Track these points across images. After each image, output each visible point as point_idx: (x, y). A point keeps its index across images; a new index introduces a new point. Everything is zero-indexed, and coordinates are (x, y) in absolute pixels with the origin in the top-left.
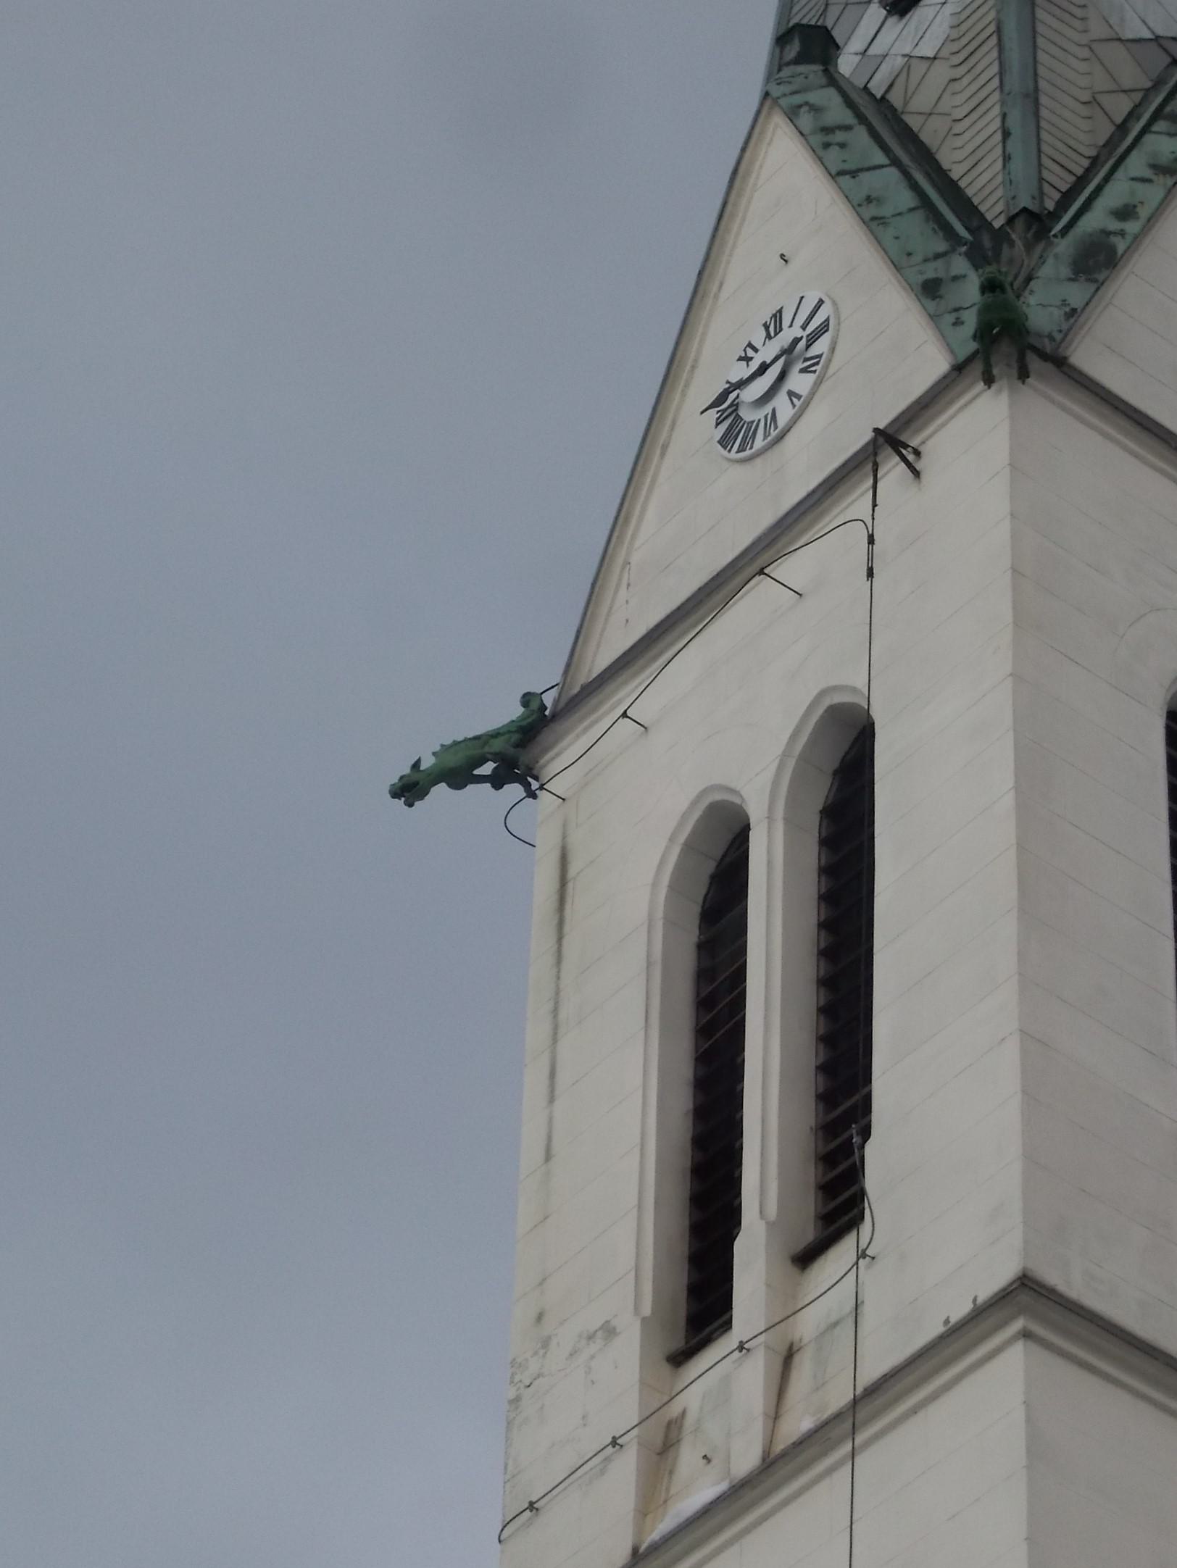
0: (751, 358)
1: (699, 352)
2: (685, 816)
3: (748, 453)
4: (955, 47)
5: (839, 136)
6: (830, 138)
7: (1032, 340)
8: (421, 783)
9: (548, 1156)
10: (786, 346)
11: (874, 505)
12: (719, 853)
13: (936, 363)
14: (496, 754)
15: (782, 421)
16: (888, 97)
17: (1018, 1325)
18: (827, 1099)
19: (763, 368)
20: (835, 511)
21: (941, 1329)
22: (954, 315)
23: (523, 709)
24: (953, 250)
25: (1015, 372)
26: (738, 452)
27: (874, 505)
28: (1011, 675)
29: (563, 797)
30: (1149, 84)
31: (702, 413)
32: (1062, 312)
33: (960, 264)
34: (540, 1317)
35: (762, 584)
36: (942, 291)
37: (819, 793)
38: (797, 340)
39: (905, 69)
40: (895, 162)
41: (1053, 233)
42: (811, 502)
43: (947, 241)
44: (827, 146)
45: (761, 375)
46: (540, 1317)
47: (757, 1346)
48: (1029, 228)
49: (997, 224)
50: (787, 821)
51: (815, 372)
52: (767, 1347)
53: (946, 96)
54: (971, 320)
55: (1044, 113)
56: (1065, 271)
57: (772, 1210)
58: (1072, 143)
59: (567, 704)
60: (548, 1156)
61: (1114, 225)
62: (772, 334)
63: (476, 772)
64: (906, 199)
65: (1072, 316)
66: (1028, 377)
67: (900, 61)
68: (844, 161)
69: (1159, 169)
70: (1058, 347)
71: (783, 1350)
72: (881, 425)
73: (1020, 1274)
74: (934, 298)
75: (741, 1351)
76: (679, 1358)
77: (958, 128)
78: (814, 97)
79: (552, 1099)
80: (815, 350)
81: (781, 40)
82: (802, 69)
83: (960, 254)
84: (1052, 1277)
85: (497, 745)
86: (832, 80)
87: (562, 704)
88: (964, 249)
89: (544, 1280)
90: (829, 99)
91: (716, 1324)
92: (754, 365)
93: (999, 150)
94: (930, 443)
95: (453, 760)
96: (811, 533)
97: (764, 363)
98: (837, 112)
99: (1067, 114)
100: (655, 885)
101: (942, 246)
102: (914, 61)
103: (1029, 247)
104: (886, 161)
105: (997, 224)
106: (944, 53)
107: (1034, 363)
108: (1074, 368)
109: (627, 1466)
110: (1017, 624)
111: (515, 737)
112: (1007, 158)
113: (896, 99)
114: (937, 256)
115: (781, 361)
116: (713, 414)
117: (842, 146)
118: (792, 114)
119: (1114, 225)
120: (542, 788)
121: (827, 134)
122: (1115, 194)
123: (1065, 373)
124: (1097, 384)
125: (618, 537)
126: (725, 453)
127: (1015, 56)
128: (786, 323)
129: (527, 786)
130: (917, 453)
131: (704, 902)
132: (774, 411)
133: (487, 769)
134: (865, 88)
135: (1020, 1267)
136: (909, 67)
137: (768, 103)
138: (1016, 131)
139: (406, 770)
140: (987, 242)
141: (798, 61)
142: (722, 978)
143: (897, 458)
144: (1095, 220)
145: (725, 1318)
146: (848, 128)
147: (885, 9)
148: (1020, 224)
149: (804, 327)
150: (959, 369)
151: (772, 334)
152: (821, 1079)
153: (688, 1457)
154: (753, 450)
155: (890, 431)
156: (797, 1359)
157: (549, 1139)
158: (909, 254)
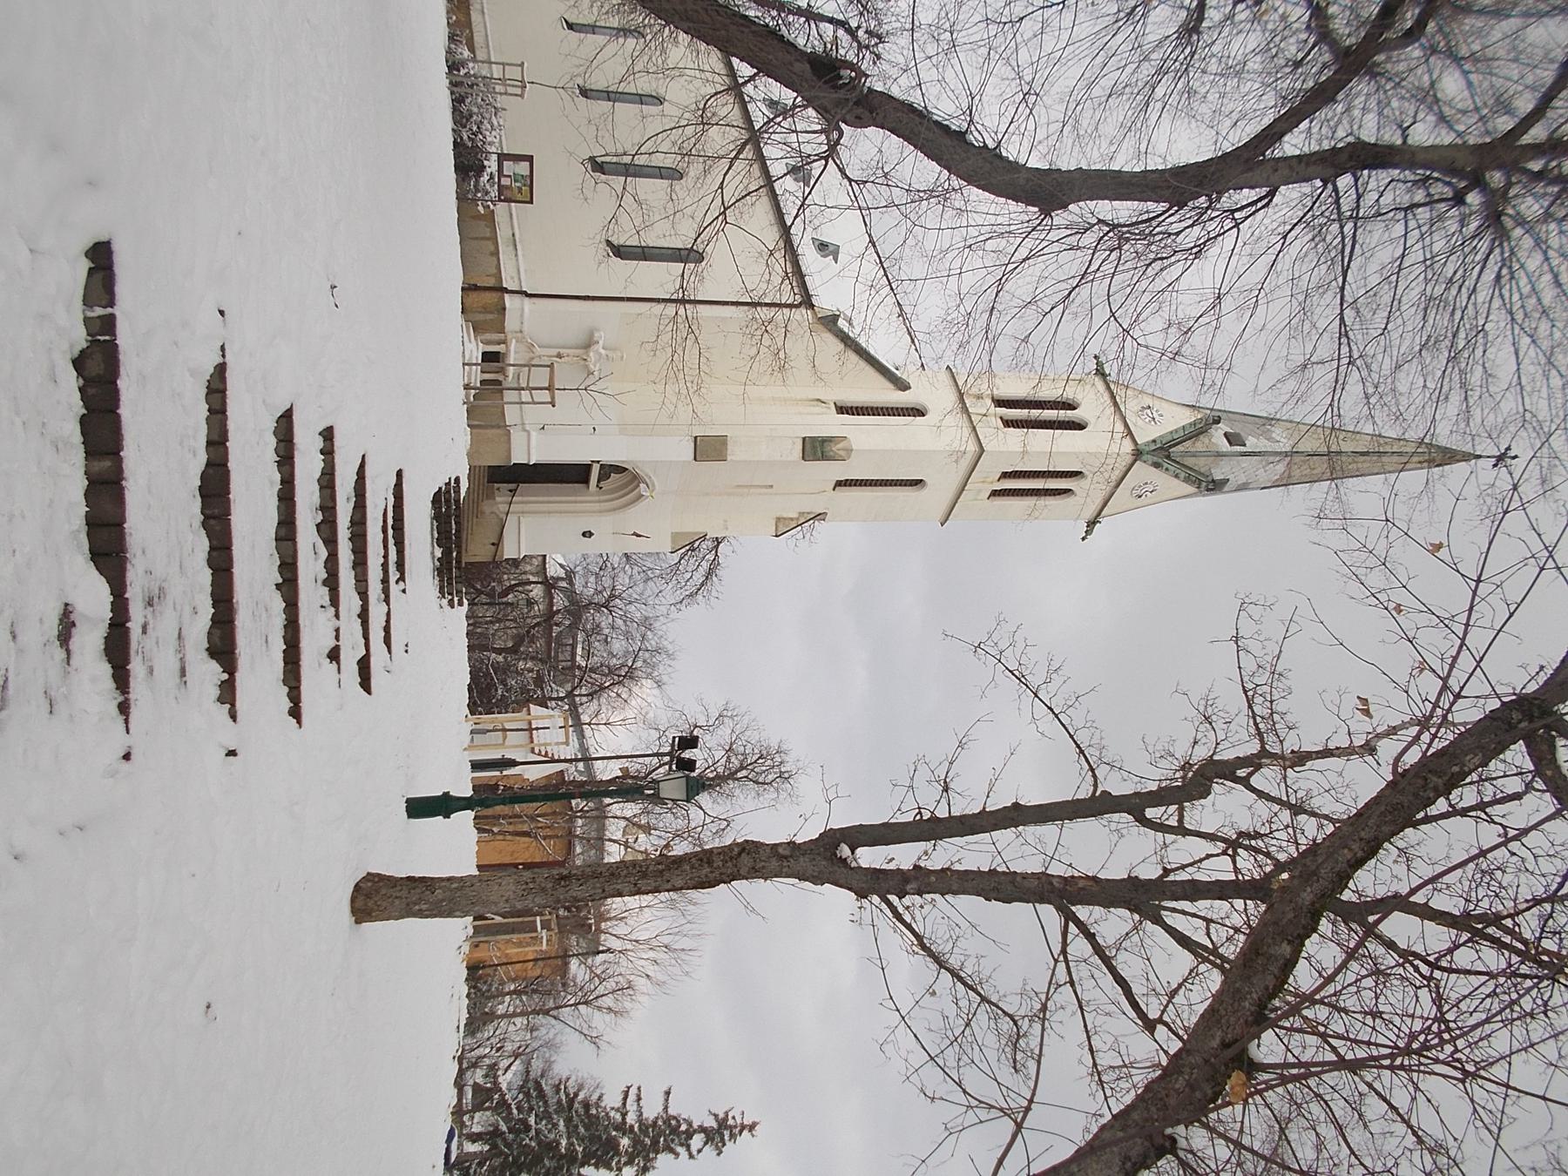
34: (208, 1007)
144: (1166, 465)
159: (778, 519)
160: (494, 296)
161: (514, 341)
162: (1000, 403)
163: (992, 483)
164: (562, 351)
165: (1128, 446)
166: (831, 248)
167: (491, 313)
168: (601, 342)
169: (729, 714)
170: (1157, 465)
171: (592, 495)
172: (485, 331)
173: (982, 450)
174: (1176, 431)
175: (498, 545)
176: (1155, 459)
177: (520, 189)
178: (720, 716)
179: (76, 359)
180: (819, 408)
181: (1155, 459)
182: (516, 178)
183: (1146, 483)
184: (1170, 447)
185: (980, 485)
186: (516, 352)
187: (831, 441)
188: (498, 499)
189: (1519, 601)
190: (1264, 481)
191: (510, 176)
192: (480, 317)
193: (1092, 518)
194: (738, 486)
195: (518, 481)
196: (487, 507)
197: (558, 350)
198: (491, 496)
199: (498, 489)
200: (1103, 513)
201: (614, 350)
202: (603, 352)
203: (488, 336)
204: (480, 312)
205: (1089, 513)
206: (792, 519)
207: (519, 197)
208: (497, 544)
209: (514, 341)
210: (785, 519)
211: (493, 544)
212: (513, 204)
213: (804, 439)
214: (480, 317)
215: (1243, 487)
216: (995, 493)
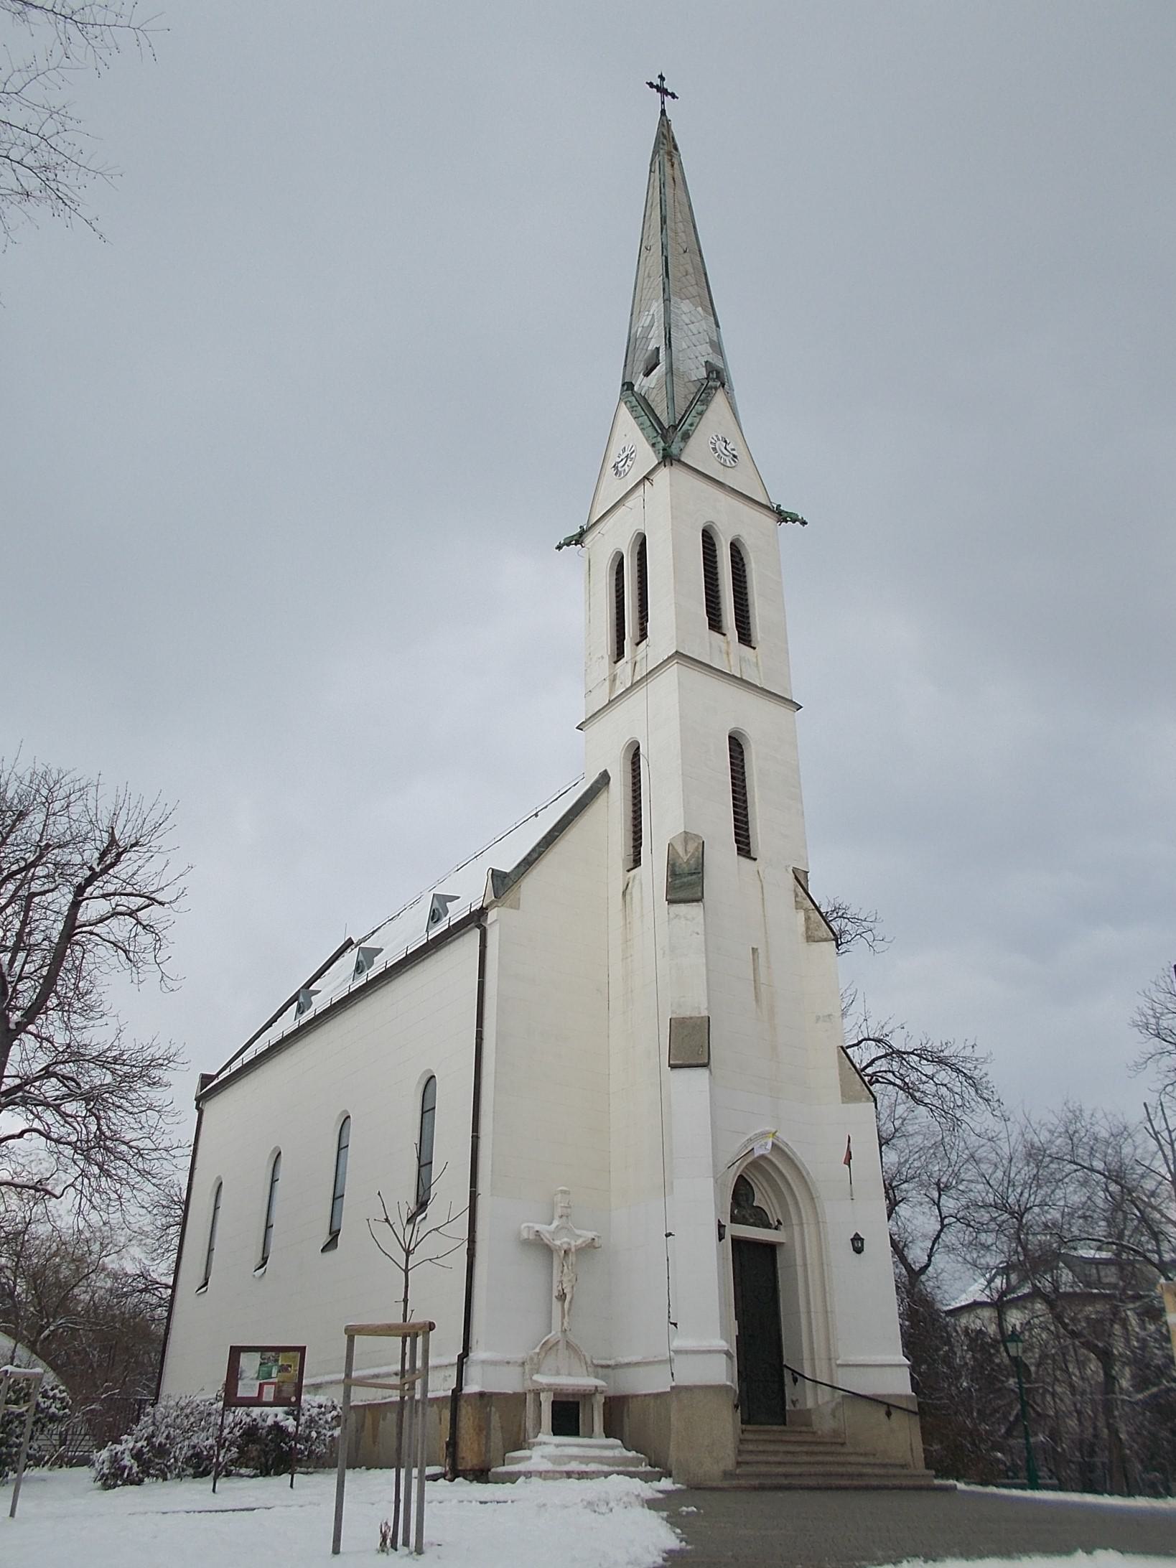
18: (641, 612)
29: (530, 885)
33: (659, 439)
54: (661, 455)
81: (623, 385)
85: (575, 538)
95: (567, 541)
98: (635, 403)
101: (655, 435)
109: (607, 683)
113: (646, 397)
118: (626, 403)
122: (689, 421)
133: (574, 542)
141: (627, 390)
150: (659, 463)
153: (618, 682)
159: (810, 938)
160: (466, 1413)
161: (536, 1377)
162: (620, 653)
163: (728, 643)
164: (555, 1293)
165: (664, 474)
166: (436, 905)
167: (488, 1419)
168: (537, 1227)
169: (1153, 1021)
170: (686, 437)
171: (792, 1238)
172: (521, 1429)
174: (640, 425)
175: (889, 1405)
176: (678, 439)
177: (283, 1369)
178: (1158, 1035)
180: (635, 890)
181: (678, 439)
182: (264, 1375)
183: (714, 449)
185: (731, 656)
186: (558, 1374)
187: (673, 865)
188: (810, 1404)
189: (1153, 1122)
190: (705, 324)
191: (261, 1386)
192: (497, 1438)
193: (774, 517)
194: (757, 1000)
195: (778, 1367)
196: (825, 1425)
197: (554, 1298)
198: (805, 1417)
199: (794, 1403)
200: (764, 502)
201: (553, 1206)
202: (555, 1223)
203: (529, 1424)
204: (488, 1437)
205: (769, 521)
206: (807, 919)
207: (294, 1371)
208: (887, 1406)
209: (536, 1377)
210: (807, 929)
211: (889, 1414)
212: (431, 1363)
213: (670, 902)
214: (497, 1438)
215: (717, 347)
216: (745, 637)
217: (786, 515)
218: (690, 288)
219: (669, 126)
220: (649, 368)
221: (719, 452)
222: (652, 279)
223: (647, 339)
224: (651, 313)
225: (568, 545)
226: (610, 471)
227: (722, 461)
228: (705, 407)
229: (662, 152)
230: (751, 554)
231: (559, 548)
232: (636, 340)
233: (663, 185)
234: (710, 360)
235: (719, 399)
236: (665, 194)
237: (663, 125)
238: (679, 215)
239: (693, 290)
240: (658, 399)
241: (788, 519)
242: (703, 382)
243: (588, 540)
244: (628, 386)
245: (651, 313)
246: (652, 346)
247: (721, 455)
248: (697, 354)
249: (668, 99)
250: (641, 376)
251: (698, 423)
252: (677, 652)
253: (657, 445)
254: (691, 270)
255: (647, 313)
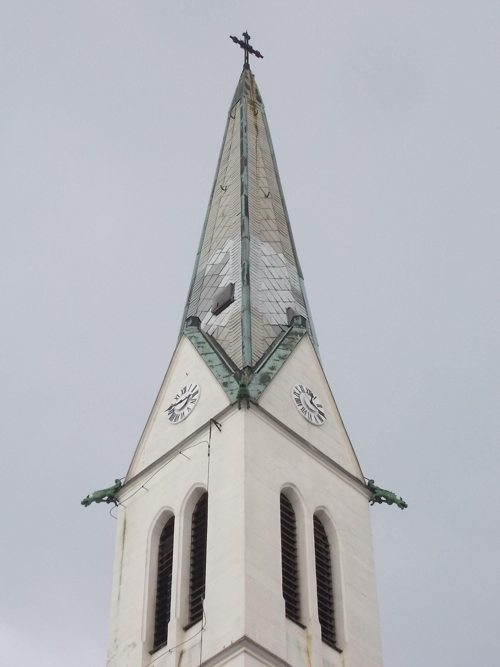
0: (178, 399)
1: (164, 396)
2: (157, 514)
3: (176, 422)
4: (230, 324)
5: (202, 345)
6: (199, 345)
7: (251, 399)
8: (89, 502)
9: (119, 599)
10: (187, 396)
11: (210, 438)
12: (165, 523)
13: (226, 403)
14: (108, 495)
15: (186, 415)
16: (213, 335)
17: (243, 649)
18: (192, 588)
19: (181, 401)
20: (201, 437)
21: (223, 649)
22: (231, 391)
23: (116, 484)
24: (231, 375)
25: (246, 407)
26: (174, 422)
27: (210, 438)
28: (244, 483)
30: (277, 336)
31: (165, 411)
32: (258, 392)
33: (232, 379)
34: (116, 640)
35: (179, 456)
36: (228, 386)
37: (192, 509)
38: (190, 395)
39: (217, 329)
40: (216, 352)
41: (255, 372)
42: (193, 435)
43: (229, 373)
44: (199, 347)
45: (181, 403)
46: (116, 640)
47: (174, 651)
48: (248, 371)
49: (240, 369)
50: (184, 516)
51: (194, 403)
52: (176, 651)
53: (228, 335)
54: (236, 393)
55: (252, 342)
56: (258, 382)
57: (178, 616)
58: (259, 350)
59: (127, 483)
60: (119, 599)
61: (270, 371)
62: (184, 393)
63: (103, 499)
64: (218, 361)
65: (260, 393)
66: (249, 408)
67: (216, 327)
68: (203, 351)
69: (280, 358)
70: (256, 401)
71: (180, 652)
72: (211, 418)
73: (244, 636)
74: (226, 387)
75: (169, 652)
76: (152, 653)
77: (231, 344)
78: (195, 335)
79: (120, 584)
80: (194, 398)
82: (192, 327)
83: (232, 376)
84: (251, 637)
85: (109, 492)
86: (200, 331)
87: (126, 482)
88: (233, 375)
89: (117, 630)
90: (199, 335)
91: (163, 644)
92: (179, 401)
93: (242, 350)
94: (224, 423)
95: (98, 496)
96: (191, 444)
97: (181, 400)
98: (201, 339)
99: (258, 343)
100: (149, 530)
101: (228, 374)
102: (219, 327)
103: (249, 375)
104: (214, 352)
105: (240, 369)
106: (227, 326)
107: (251, 405)
108: (260, 406)
110: (245, 470)
111: (113, 491)
112: (243, 353)
113: (215, 336)
114: (226, 376)
115: (186, 400)
116: (168, 412)
117: (203, 347)
118: (190, 338)
119: (270, 371)
120: (120, 504)
121: (199, 344)
122: (270, 363)
123: (258, 408)
124: (265, 410)
125: (142, 441)
126: (170, 422)
127: (246, 327)
128: (187, 390)
129: (116, 503)
130: (221, 425)
131: (161, 535)
132: (183, 412)
134: (207, 332)
135: (244, 634)
136: (218, 328)
137: (184, 335)
138: (246, 346)
139: (86, 498)
140: (238, 374)
141: (191, 325)
142: (164, 556)
143: (216, 426)
144: (265, 370)
145: (166, 642)
146: (204, 343)
147: (212, 313)
148: (246, 369)
149: (192, 392)
150: (232, 405)
151: (184, 393)
152: (191, 583)
154: (178, 422)
155: (214, 419)
156: (184, 655)
157: (119, 594)
158: (219, 376)
163: (308, 638)
170: (266, 380)
173: (229, 333)
179: (306, 320)
183: (298, 401)
184: (236, 368)
185: (313, 656)
190: (287, 272)
215: (301, 298)
217: (380, 493)
218: (272, 233)
219: (252, 81)
220: (220, 305)
221: (304, 405)
222: (227, 218)
223: (217, 276)
224: (225, 250)
225: (98, 500)
226: (162, 414)
227: (307, 416)
228: (288, 352)
229: (244, 100)
230: (337, 532)
231: (86, 503)
232: (204, 277)
233: (244, 130)
234: (292, 307)
235: (304, 347)
236: (246, 138)
237: (247, 78)
238: (261, 161)
239: (276, 236)
240: (231, 338)
241: (383, 498)
242: (284, 328)
243: (125, 497)
244: (194, 321)
245: (225, 250)
246: (225, 282)
247: (305, 407)
248: (279, 299)
249: (252, 56)
250: (210, 314)
251: (280, 368)
252: (245, 641)
253: (229, 385)
254: (272, 216)
255: (219, 251)
